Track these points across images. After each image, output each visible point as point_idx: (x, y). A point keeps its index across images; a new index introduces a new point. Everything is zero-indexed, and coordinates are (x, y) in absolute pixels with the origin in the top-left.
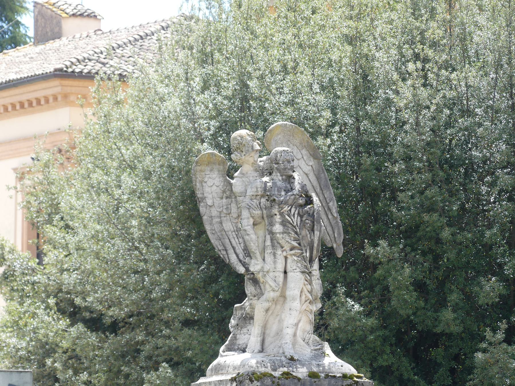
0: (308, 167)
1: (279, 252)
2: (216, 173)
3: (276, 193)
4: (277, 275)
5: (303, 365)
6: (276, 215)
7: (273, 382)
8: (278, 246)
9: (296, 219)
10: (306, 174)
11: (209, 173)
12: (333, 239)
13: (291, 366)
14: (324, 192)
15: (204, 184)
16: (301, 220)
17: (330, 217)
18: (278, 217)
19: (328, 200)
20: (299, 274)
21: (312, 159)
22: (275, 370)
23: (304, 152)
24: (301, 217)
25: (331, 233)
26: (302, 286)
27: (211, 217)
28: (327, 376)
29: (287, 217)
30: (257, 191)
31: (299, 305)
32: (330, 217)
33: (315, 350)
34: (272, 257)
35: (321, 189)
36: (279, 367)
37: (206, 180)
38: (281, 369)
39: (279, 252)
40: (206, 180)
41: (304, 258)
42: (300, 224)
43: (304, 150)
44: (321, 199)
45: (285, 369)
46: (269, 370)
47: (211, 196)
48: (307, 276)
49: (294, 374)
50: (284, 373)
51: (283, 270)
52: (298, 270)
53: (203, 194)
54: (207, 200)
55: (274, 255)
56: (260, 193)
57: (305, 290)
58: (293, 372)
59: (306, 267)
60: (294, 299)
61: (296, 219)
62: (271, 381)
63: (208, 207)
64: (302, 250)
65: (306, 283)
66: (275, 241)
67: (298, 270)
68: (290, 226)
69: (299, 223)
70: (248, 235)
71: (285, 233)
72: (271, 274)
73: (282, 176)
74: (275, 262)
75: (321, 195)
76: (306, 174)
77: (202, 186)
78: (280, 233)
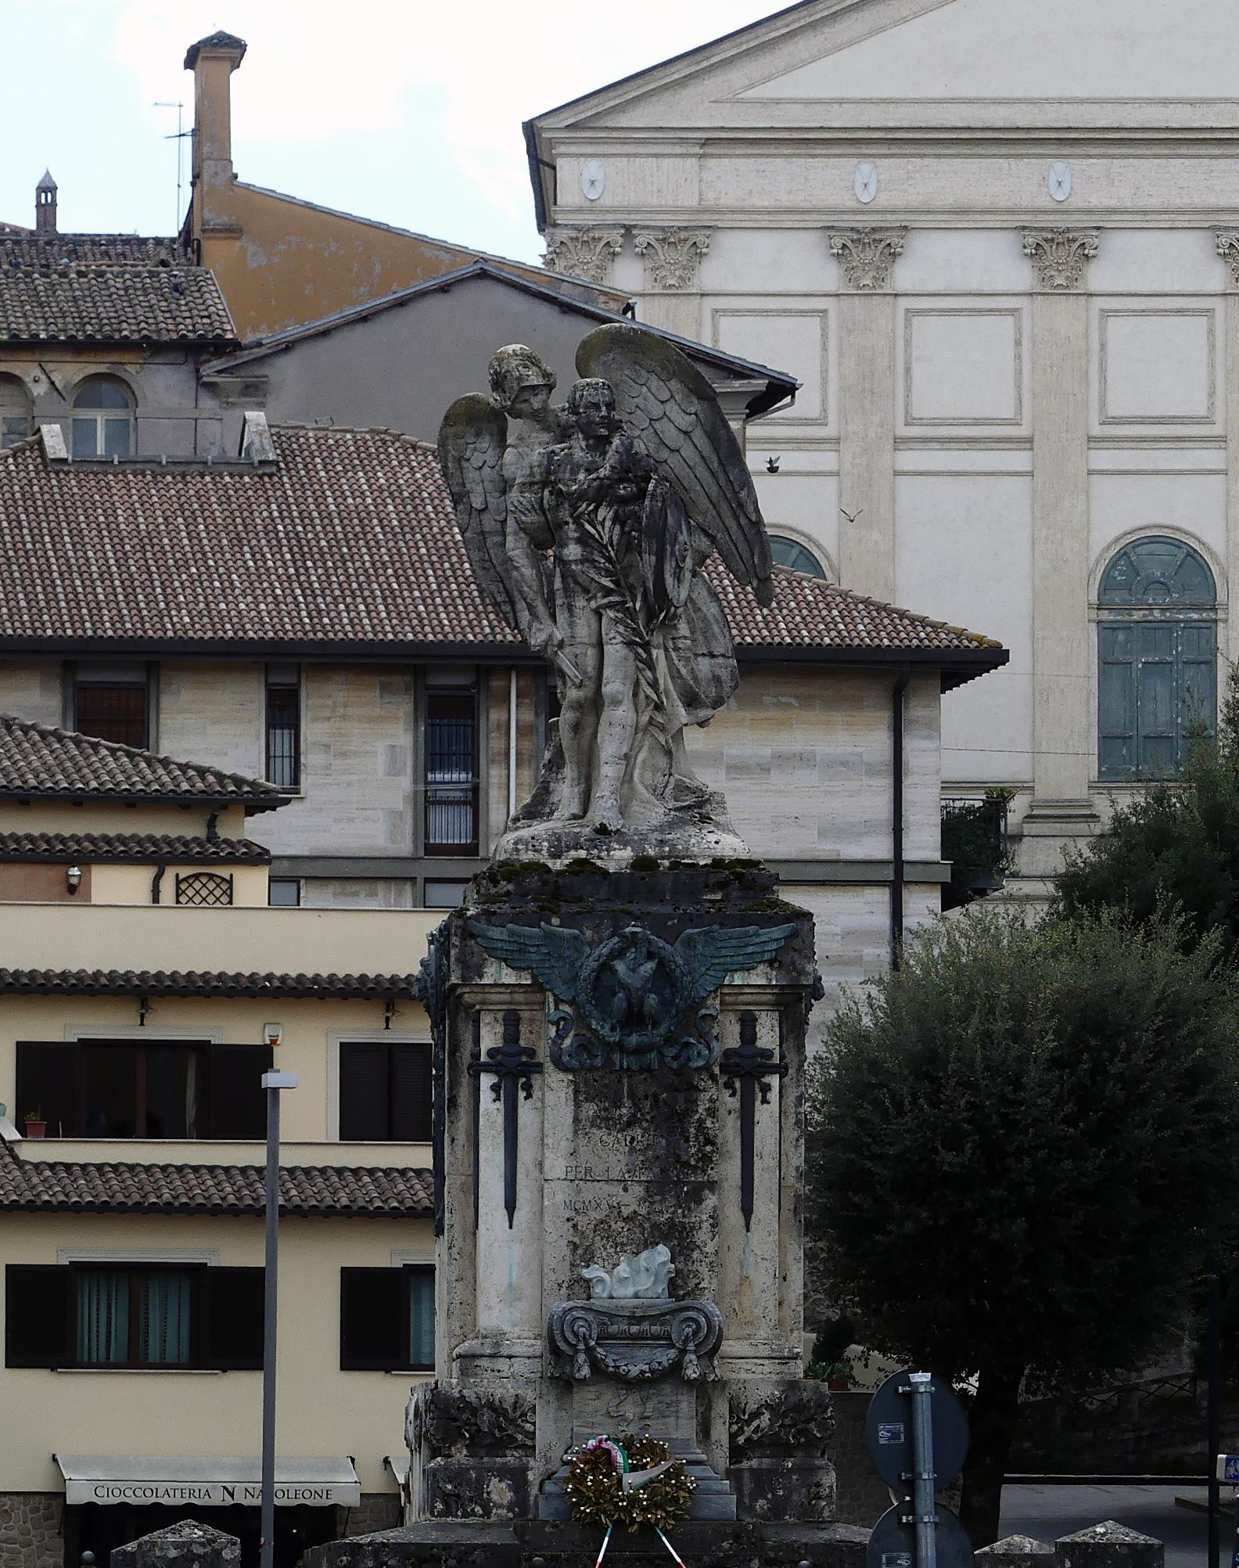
0: (687, 417)
1: (580, 602)
2: (488, 438)
3: (567, 476)
4: (578, 652)
5: (625, 844)
6: (567, 523)
7: (545, 883)
8: (578, 588)
9: (607, 529)
10: (685, 433)
11: (473, 439)
12: (751, 569)
13: (595, 847)
14: (729, 468)
15: (465, 464)
16: (622, 533)
17: (743, 521)
18: (572, 526)
19: (736, 486)
20: (619, 647)
21: (695, 400)
22: (556, 855)
23: (674, 384)
24: (623, 525)
25: (746, 555)
26: (631, 671)
27: (483, 533)
28: (675, 865)
29: (588, 527)
30: (532, 474)
31: (632, 715)
32: (743, 521)
33: (676, 809)
34: (567, 615)
35: (720, 462)
36: (569, 848)
37: (468, 454)
38: (572, 853)
39: (580, 602)
40: (468, 454)
41: (631, 614)
42: (619, 540)
43: (673, 382)
44: (723, 484)
45: (582, 854)
46: (544, 858)
47: (480, 489)
48: (640, 651)
49: (599, 863)
50: (578, 862)
51: (594, 640)
52: (619, 639)
53: (464, 485)
54: (473, 499)
55: (570, 608)
56: (538, 477)
57: (643, 681)
58: (600, 858)
59: (636, 631)
60: (617, 703)
61: (607, 529)
62: (540, 879)
63: (475, 513)
64: (624, 596)
65: (641, 665)
66: (570, 580)
67: (619, 639)
68: (595, 545)
69: (615, 538)
70: (516, 568)
71: (587, 560)
72: (567, 649)
73: (586, 438)
74: (572, 625)
75: (721, 476)
76: (685, 433)
77: (461, 469)
78: (575, 562)
